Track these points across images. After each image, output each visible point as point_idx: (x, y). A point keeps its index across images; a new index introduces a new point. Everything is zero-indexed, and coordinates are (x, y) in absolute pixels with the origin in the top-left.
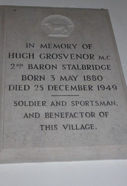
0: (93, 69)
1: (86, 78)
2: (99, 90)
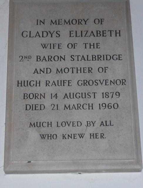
0: (104, 60)
1: (104, 95)
2: (100, 108)
